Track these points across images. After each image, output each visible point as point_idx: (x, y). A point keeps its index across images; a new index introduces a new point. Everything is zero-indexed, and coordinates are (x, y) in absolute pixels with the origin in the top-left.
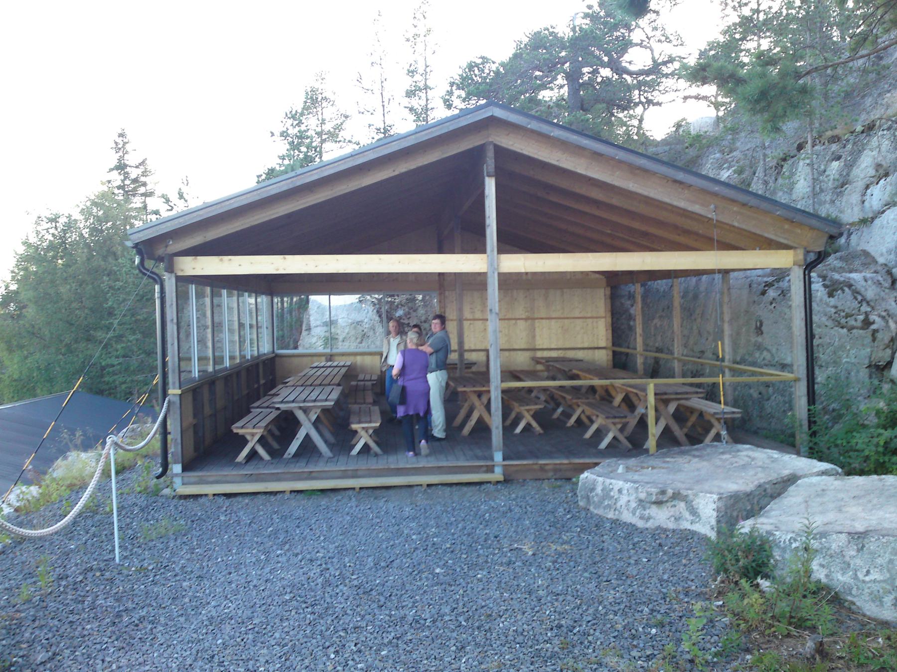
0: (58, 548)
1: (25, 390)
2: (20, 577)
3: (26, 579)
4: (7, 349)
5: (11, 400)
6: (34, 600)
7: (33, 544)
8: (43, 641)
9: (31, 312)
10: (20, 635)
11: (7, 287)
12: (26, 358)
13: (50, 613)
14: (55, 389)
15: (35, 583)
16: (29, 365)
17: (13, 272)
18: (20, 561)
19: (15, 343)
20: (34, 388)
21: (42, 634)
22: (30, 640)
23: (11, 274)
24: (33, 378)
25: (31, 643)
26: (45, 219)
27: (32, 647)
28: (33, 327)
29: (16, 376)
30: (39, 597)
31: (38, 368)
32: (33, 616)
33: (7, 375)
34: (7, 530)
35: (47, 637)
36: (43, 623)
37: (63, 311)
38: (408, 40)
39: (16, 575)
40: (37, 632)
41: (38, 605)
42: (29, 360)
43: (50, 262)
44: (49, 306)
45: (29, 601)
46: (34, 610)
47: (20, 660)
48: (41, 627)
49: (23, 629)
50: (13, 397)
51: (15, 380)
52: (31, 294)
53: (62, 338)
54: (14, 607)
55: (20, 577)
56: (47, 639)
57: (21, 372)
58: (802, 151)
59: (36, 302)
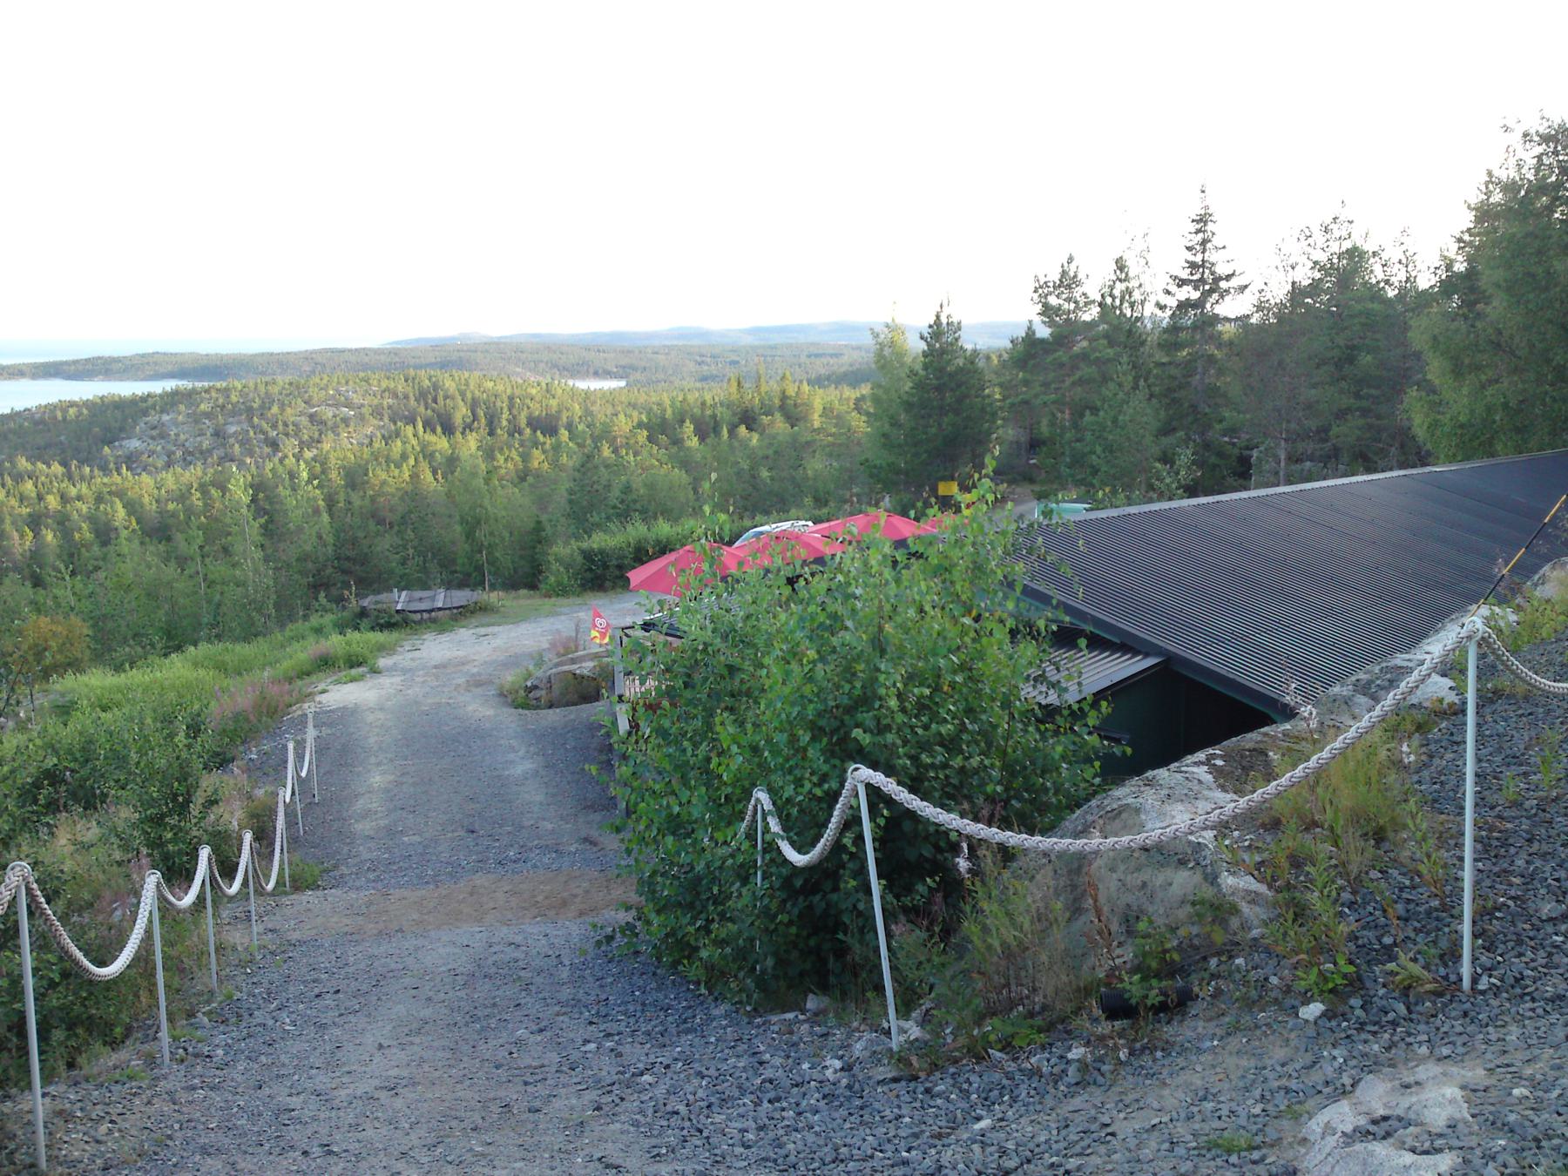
0: (1562, 723)
1: (1476, 443)
2: (1498, 759)
3: (1508, 765)
4: (1453, 371)
5: (1452, 459)
6: (1527, 804)
7: (1514, 708)
8: (1550, 881)
9: (1497, 308)
10: (1508, 860)
11: (1449, 267)
12: (1483, 387)
13: (1559, 835)
14: (1530, 446)
15: (1525, 774)
16: (1489, 398)
17: (1460, 240)
18: (1495, 732)
19: (1467, 361)
20: (1490, 442)
21: (1548, 868)
22: (1525, 873)
23: (1457, 245)
24: (1494, 422)
25: (1529, 878)
26: (1536, 139)
27: (1530, 887)
28: (1500, 333)
29: (1462, 419)
30: (1535, 802)
31: (1505, 406)
32: (1527, 832)
33: (1448, 416)
34: (1513, 672)
35: (1556, 875)
36: (1545, 848)
37: (1557, 305)
38: (1507, 129)
39: (1491, 754)
40: (1538, 863)
41: (1535, 815)
42: (1490, 391)
43: (1538, 215)
44: (1531, 296)
45: (1516, 804)
46: (1528, 822)
47: (1510, 903)
48: (1544, 856)
49: (1512, 850)
50: (1454, 455)
51: (1462, 426)
52: (1500, 274)
53: (1551, 355)
54: (1492, 808)
55: (1498, 759)
56: (1557, 880)
57: (1472, 411)
58: (586, 668)
59: (1508, 290)
